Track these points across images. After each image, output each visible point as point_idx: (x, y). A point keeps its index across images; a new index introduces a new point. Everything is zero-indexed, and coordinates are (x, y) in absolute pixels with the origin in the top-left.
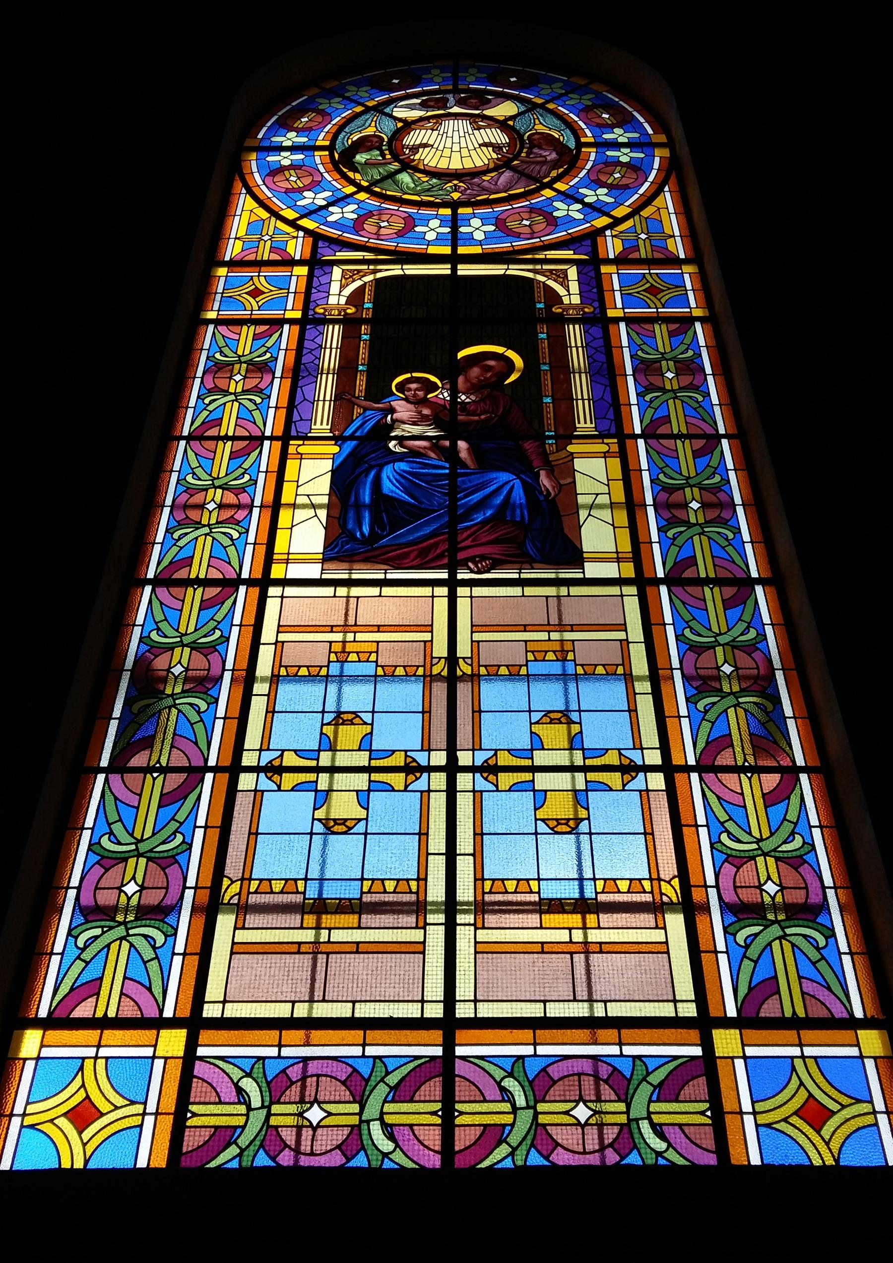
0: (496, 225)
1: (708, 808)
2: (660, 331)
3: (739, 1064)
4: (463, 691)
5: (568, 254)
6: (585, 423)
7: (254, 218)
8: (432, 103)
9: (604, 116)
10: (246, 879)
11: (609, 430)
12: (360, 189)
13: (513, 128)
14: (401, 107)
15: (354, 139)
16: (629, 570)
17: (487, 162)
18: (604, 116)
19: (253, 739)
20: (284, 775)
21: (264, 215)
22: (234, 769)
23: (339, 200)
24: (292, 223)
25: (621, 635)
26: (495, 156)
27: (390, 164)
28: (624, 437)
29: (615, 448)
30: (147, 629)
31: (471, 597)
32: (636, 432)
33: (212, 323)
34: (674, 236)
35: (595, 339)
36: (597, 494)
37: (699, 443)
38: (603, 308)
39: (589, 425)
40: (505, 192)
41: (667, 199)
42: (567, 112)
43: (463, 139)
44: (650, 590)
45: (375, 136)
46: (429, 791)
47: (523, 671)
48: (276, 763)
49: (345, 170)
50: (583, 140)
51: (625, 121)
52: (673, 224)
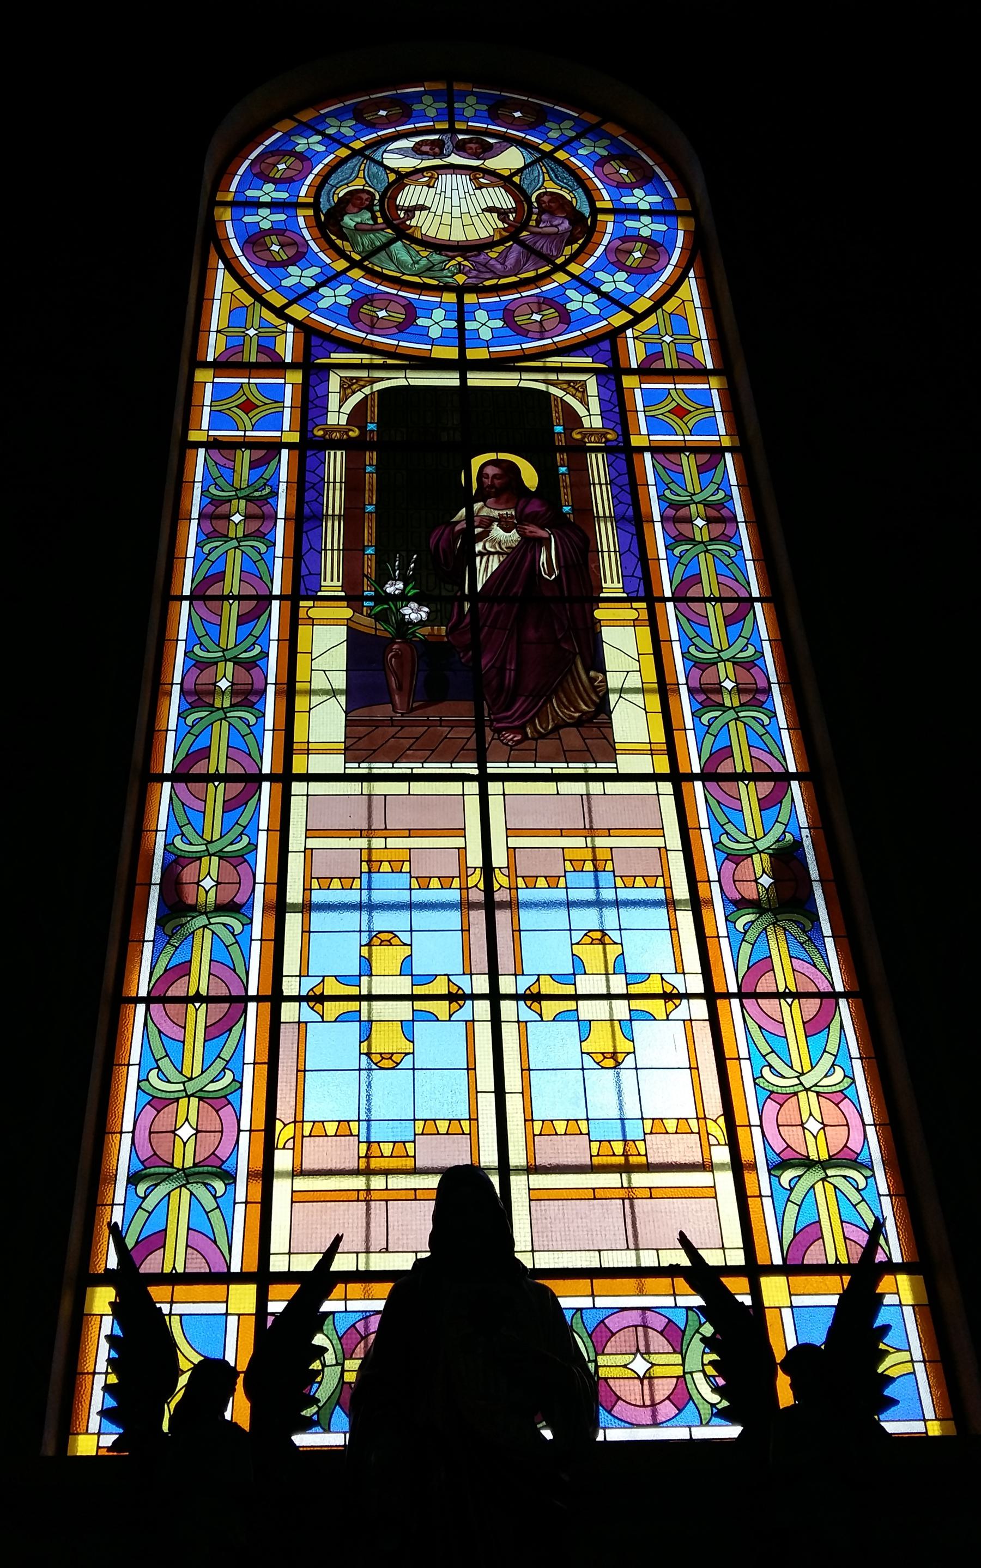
0: (503, 319)
1: (750, 1039)
2: (688, 463)
3: (787, 1313)
4: (502, 917)
5: (586, 361)
6: (612, 582)
7: (236, 304)
8: (426, 148)
9: (622, 171)
10: (298, 1121)
11: (637, 591)
12: (354, 264)
13: (519, 187)
14: (392, 151)
15: (340, 195)
16: (663, 766)
17: (492, 233)
18: (622, 171)
19: (291, 964)
20: (325, 1003)
21: (247, 299)
22: (275, 998)
23: (331, 279)
24: (280, 312)
25: (659, 842)
26: (500, 225)
27: (382, 230)
28: (652, 599)
29: (644, 615)
30: (171, 833)
31: (504, 795)
32: (672, 604)
33: (202, 447)
34: (700, 339)
35: (620, 475)
36: (628, 672)
37: (731, 607)
38: (626, 435)
39: (616, 585)
40: (515, 275)
41: (691, 289)
42: (580, 165)
43: (463, 201)
44: (685, 786)
45: (363, 191)
46: (473, 1021)
47: (562, 883)
48: (318, 991)
49: (334, 237)
50: (599, 205)
51: (645, 179)
52: (699, 324)
